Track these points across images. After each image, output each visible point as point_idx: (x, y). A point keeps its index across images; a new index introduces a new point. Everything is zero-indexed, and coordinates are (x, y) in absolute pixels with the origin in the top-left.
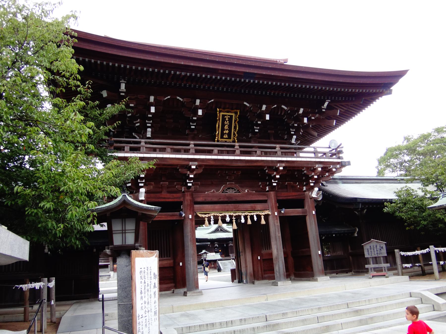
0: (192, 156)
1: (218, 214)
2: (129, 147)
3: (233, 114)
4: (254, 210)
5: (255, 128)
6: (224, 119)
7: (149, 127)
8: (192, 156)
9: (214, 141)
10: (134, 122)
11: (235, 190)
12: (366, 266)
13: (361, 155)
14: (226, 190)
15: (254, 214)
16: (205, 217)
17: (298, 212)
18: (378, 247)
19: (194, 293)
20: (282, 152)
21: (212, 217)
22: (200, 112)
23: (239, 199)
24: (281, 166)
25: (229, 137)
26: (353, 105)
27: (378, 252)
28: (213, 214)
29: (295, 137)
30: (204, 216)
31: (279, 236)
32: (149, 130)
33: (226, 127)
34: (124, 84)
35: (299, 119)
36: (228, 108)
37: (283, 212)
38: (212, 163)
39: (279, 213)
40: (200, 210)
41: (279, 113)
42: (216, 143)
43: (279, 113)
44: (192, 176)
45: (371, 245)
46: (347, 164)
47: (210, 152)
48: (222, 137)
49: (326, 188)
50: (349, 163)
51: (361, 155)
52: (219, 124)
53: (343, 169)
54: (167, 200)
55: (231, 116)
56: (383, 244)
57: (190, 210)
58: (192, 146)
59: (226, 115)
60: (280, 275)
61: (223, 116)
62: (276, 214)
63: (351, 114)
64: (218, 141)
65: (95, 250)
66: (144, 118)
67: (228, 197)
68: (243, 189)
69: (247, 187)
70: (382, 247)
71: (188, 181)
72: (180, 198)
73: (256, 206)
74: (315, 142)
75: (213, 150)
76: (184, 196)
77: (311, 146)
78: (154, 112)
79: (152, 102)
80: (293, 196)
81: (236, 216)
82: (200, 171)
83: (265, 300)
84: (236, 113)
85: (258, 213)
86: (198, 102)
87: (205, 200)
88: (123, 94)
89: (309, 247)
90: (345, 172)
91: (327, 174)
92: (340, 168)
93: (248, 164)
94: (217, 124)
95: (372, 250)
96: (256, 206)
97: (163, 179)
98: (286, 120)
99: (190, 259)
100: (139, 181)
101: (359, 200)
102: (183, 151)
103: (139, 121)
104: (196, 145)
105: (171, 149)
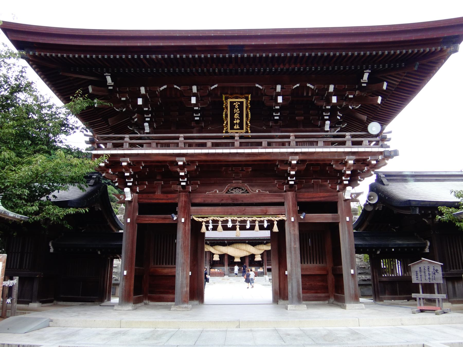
0: (181, 150)
1: (218, 219)
2: (111, 144)
3: (244, 100)
4: (265, 214)
6: (232, 107)
7: (327, 120)
8: (181, 150)
9: (223, 133)
11: (243, 190)
12: (18, 277)
14: (232, 190)
15: (265, 219)
16: (203, 222)
17: (326, 218)
18: (431, 270)
19: (180, 307)
20: (296, 142)
21: (211, 222)
23: (246, 201)
25: (241, 128)
27: (431, 277)
28: (212, 218)
30: (200, 220)
31: (295, 248)
32: (328, 123)
33: (236, 116)
34: (109, 77)
36: (237, 94)
37: (302, 217)
38: (204, 158)
39: (298, 218)
40: (196, 213)
41: (305, 94)
42: (224, 135)
43: (305, 94)
44: (293, 173)
45: (422, 265)
46: (392, 154)
47: (203, 145)
48: (232, 128)
49: (386, 187)
50: (395, 153)
53: (389, 162)
54: (161, 201)
55: (242, 103)
56: (438, 265)
57: (184, 212)
58: (127, 139)
59: (235, 102)
60: (292, 297)
61: (232, 103)
62: (293, 219)
63: (415, 87)
64: (227, 132)
67: (232, 199)
68: (254, 190)
69: (259, 186)
70: (437, 270)
71: (344, 178)
72: (175, 199)
73: (268, 209)
75: (362, 141)
76: (179, 197)
80: (321, 197)
81: (224, 220)
82: (303, 167)
83: (237, 327)
84: (247, 98)
85: (270, 218)
87: (204, 201)
89: (341, 264)
92: (383, 159)
93: (248, 159)
95: (423, 274)
96: (268, 209)
97: (158, 178)
99: (179, 268)
101: (414, 203)
103: (150, 115)
104: (185, 138)
105: (324, 142)
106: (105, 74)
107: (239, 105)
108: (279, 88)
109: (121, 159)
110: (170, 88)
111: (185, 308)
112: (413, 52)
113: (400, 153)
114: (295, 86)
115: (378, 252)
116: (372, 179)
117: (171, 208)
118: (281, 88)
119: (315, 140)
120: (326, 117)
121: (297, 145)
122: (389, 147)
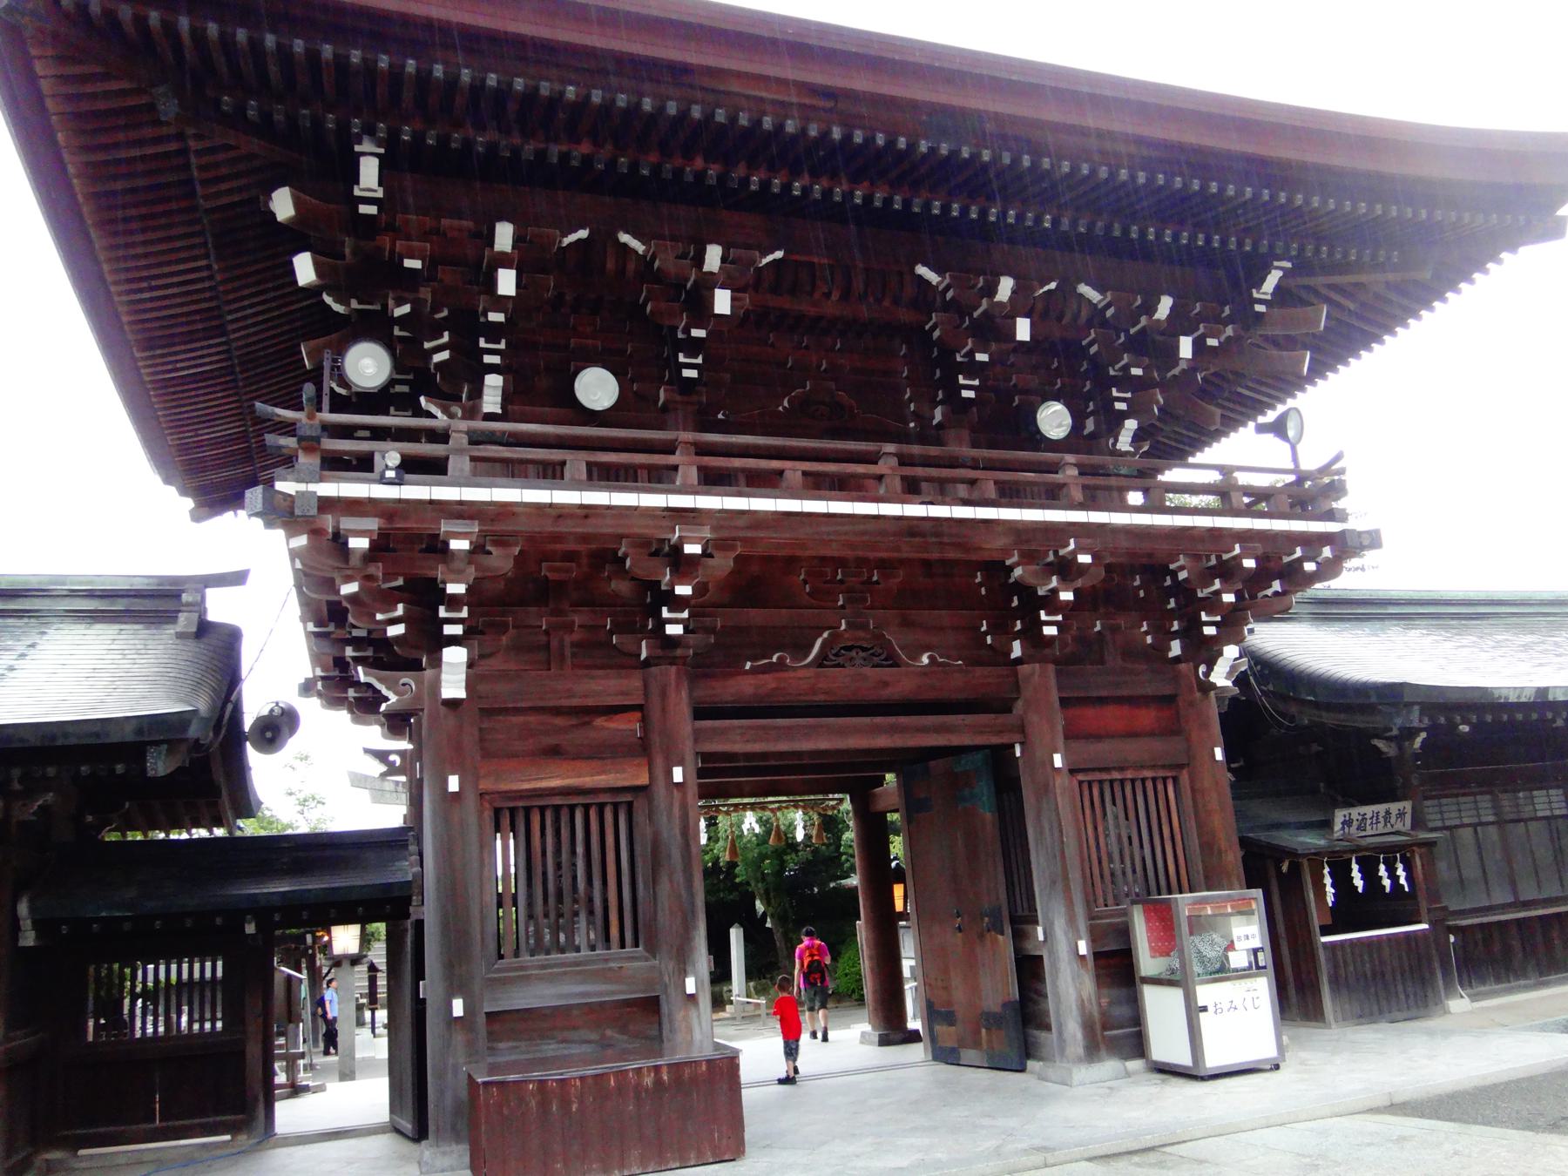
5: (962, 381)
7: (493, 369)
10: (427, 345)
22: (722, 302)
24: (692, 541)
29: (1131, 425)
32: (494, 382)
34: (375, 162)
35: (1157, 347)
44: (683, 590)
50: (1372, 540)
65: (250, 929)
66: (467, 329)
71: (665, 613)
74: (1209, 445)
75: (781, 473)
77: (1191, 460)
78: (728, 312)
79: (711, 273)
86: (713, 257)
88: (371, 210)
90: (1351, 580)
91: (1277, 586)
98: (1094, 349)
100: (443, 613)
102: (643, 474)
103: (446, 338)
106: (357, 148)
109: (445, 527)
110: (603, 240)
113: (1385, 538)
114: (770, 258)
118: (724, 260)
119: (775, 464)
120: (489, 359)
121: (590, 477)
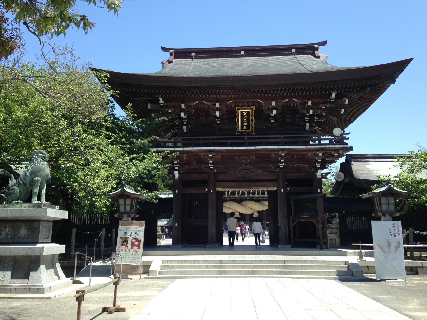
3: (250, 110)
7: (307, 122)
12: (105, 229)
13: (381, 141)
26: (379, 87)
32: (308, 125)
33: (245, 120)
36: (245, 106)
41: (292, 105)
43: (292, 105)
44: (282, 161)
48: (242, 128)
51: (381, 141)
52: (238, 118)
55: (249, 112)
61: (242, 112)
84: (252, 109)
94: (237, 119)
107: (246, 113)
108: (274, 103)
111: (215, 246)
112: (362, 84)
113: (127, 310)
115: (344, 212)
116: (343, 160)
117: (204, 183)
122: (347, 144)
